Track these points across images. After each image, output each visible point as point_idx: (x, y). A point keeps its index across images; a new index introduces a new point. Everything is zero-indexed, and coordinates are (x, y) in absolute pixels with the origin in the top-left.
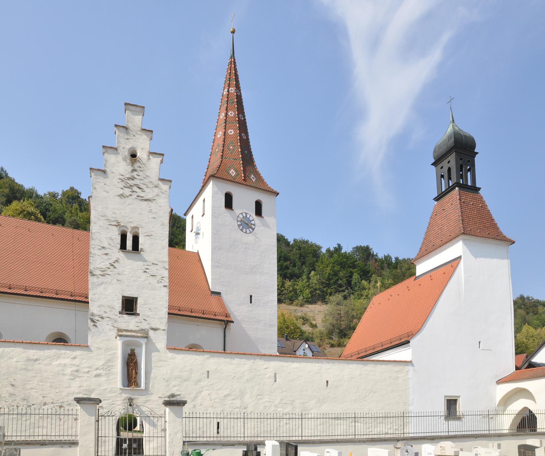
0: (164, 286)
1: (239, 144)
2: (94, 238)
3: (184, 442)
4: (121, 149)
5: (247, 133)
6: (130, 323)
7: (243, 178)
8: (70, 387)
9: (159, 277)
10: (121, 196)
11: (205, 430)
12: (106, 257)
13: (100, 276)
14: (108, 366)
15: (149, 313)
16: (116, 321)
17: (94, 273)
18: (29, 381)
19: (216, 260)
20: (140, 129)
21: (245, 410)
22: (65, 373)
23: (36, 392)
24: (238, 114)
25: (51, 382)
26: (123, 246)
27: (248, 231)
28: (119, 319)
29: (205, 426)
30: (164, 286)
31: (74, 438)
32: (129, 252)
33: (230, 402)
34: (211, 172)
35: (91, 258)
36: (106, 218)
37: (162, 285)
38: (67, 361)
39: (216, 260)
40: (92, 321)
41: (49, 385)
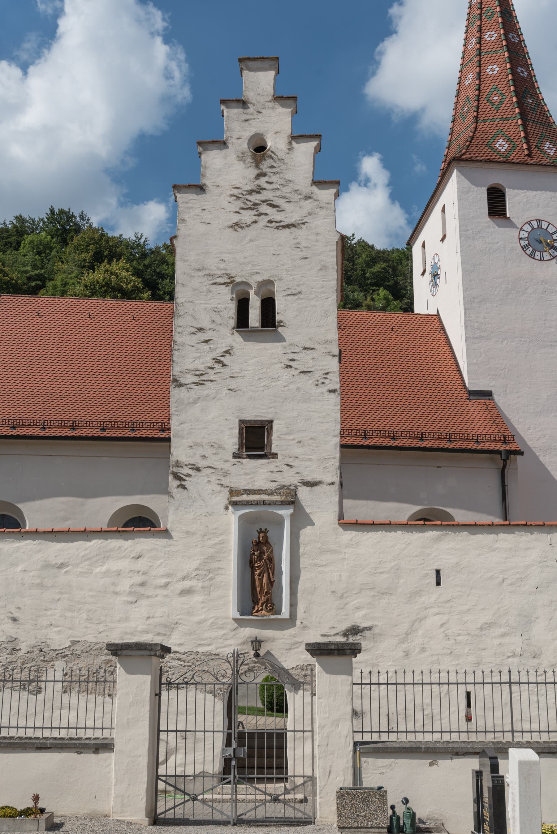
0: (330, 391)
1: (512, 88)
2: (182, 313)
3: (355, 744)
4: (235, 141)
5: (527, 66)
6: (257, 475)
7: (526, 152)
8: (127, 619)
9: (318, 375)
10: (236, 226)
11: (436, 711)
12: (206, 347)
13: (193, 386)
14: (209, 571)
15: (299, 451)
16: (226, 474)
17: (182, 381)
18: (46, 609)
19: (476, 325)
20: (270, 98)
21: (536, 661)
22: (118, 589)
23: (59, 632)
24: (505, 34)
25: (89, 611)
26: (242, 321)
27: (546, 256)
28: (233, 469)
29: (436, 702)
30: (330, 391)
31: (106, 734)
32: (255, 331)
33: (497, 642)
34: (451, 155)
35: (176, 353)
36: (207, 272)
37: (324, 389)
38: (124, 564)
39: (476, 325)
40: (177, 477)
41: (84, 616)
